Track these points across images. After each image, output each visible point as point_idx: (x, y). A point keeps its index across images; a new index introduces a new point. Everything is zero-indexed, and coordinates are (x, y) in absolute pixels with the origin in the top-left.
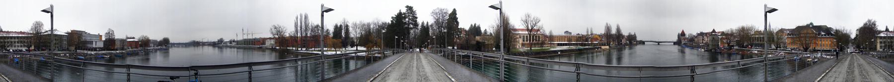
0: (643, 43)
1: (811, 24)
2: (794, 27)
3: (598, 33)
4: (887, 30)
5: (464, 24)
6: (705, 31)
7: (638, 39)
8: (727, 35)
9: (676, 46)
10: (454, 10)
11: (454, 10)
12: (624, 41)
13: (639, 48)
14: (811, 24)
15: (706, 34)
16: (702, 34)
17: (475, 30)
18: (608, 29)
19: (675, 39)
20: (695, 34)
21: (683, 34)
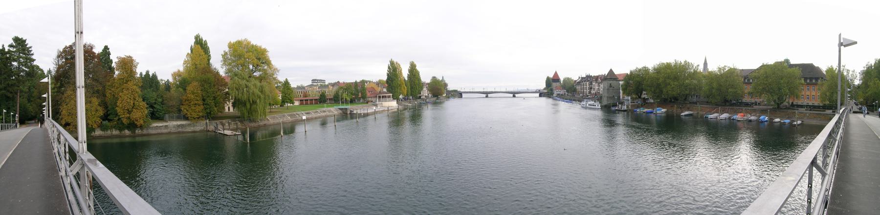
0: (459, 94)
1: (787, 61)
2: (755, 65)
3: (375, 79)
4: (324, 124)
5: (141, 70)
6: (594, 73)
7: (451, 87)
8: (748, 76)
9: (544, 99)
10: (106, 48)
11: (106, 48)
12: (425, 92)
13: (452, 104)
14: (787, 61)
15: (597, 78)
16: (589, 79)
17: (176, 75)
18: (148, 72)
19: (542, 86)
20: (575, 77)
21: (556, 79)
